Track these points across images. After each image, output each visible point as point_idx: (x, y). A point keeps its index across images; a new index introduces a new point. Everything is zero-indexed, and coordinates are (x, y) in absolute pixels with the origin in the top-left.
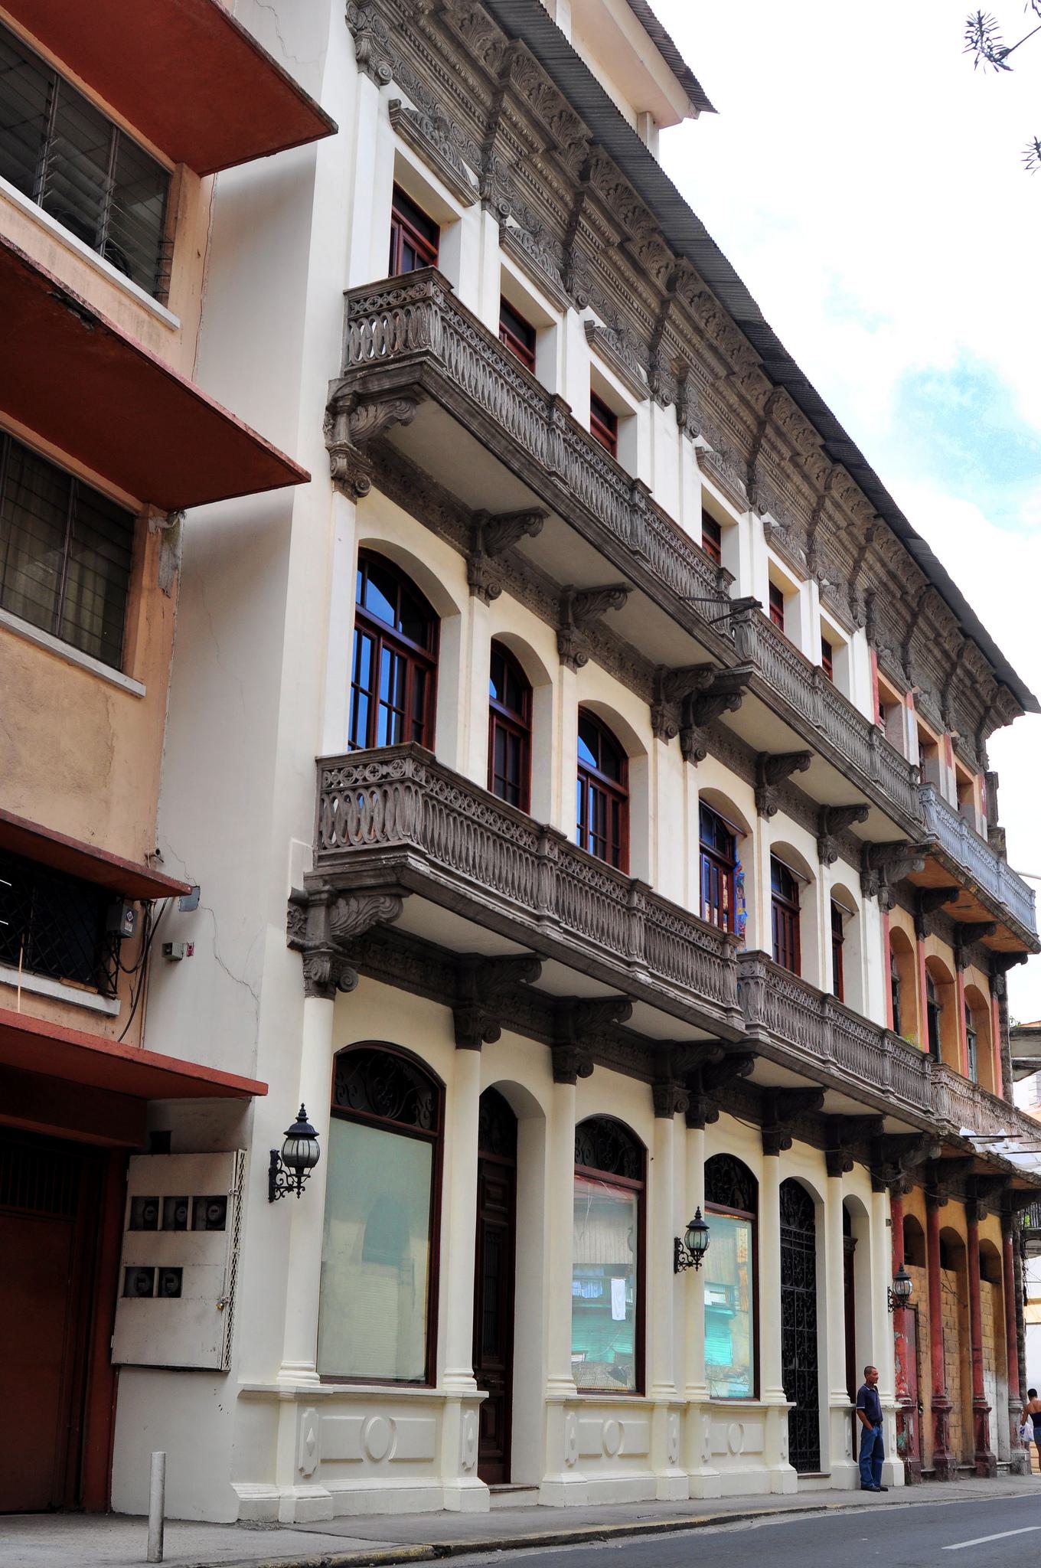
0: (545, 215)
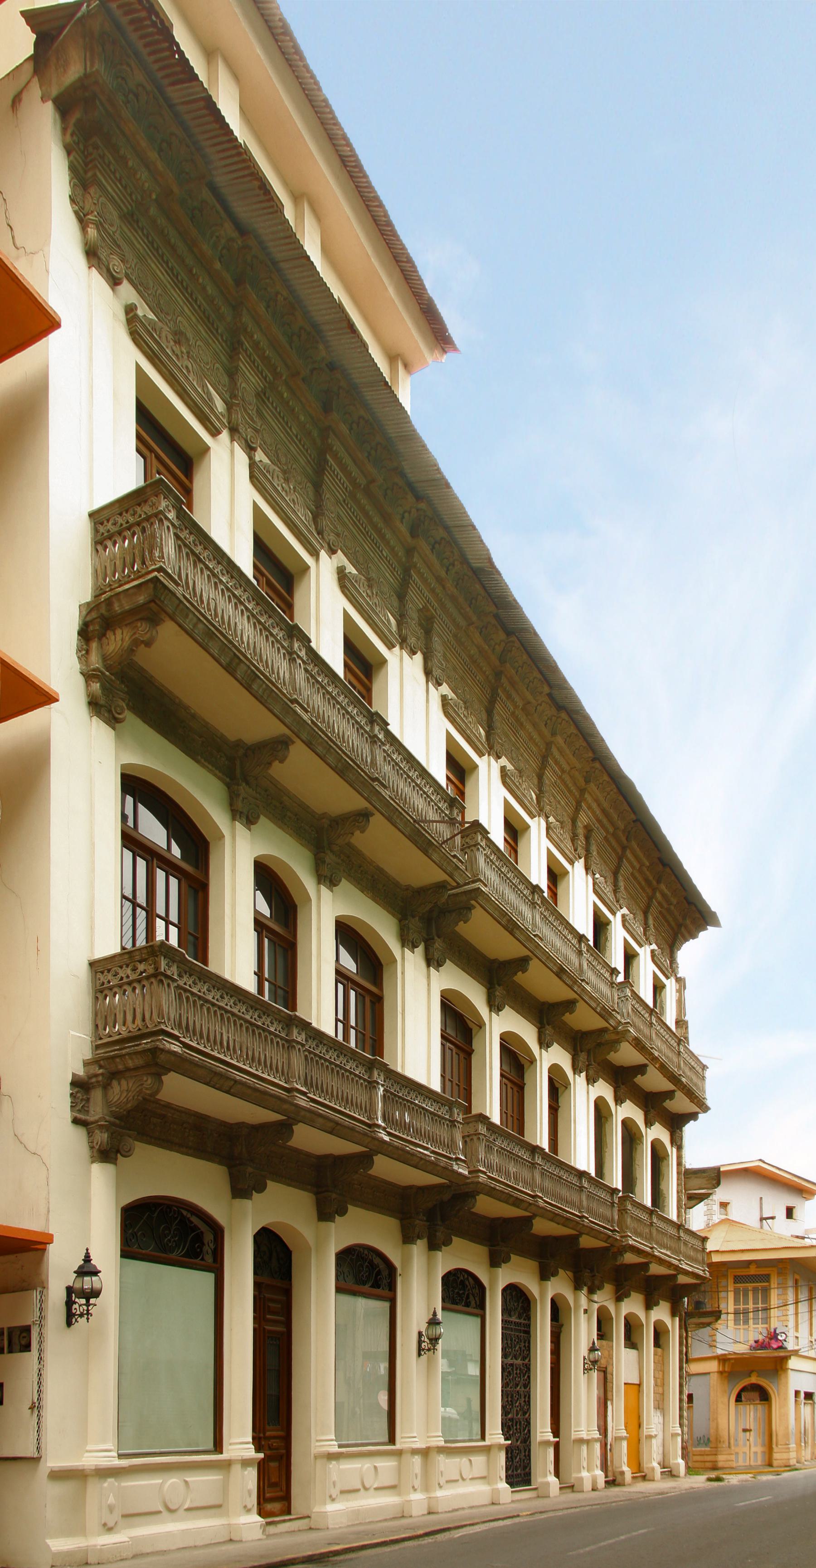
0: (295, 452)
